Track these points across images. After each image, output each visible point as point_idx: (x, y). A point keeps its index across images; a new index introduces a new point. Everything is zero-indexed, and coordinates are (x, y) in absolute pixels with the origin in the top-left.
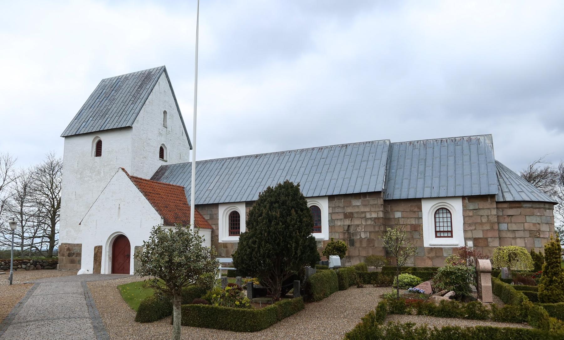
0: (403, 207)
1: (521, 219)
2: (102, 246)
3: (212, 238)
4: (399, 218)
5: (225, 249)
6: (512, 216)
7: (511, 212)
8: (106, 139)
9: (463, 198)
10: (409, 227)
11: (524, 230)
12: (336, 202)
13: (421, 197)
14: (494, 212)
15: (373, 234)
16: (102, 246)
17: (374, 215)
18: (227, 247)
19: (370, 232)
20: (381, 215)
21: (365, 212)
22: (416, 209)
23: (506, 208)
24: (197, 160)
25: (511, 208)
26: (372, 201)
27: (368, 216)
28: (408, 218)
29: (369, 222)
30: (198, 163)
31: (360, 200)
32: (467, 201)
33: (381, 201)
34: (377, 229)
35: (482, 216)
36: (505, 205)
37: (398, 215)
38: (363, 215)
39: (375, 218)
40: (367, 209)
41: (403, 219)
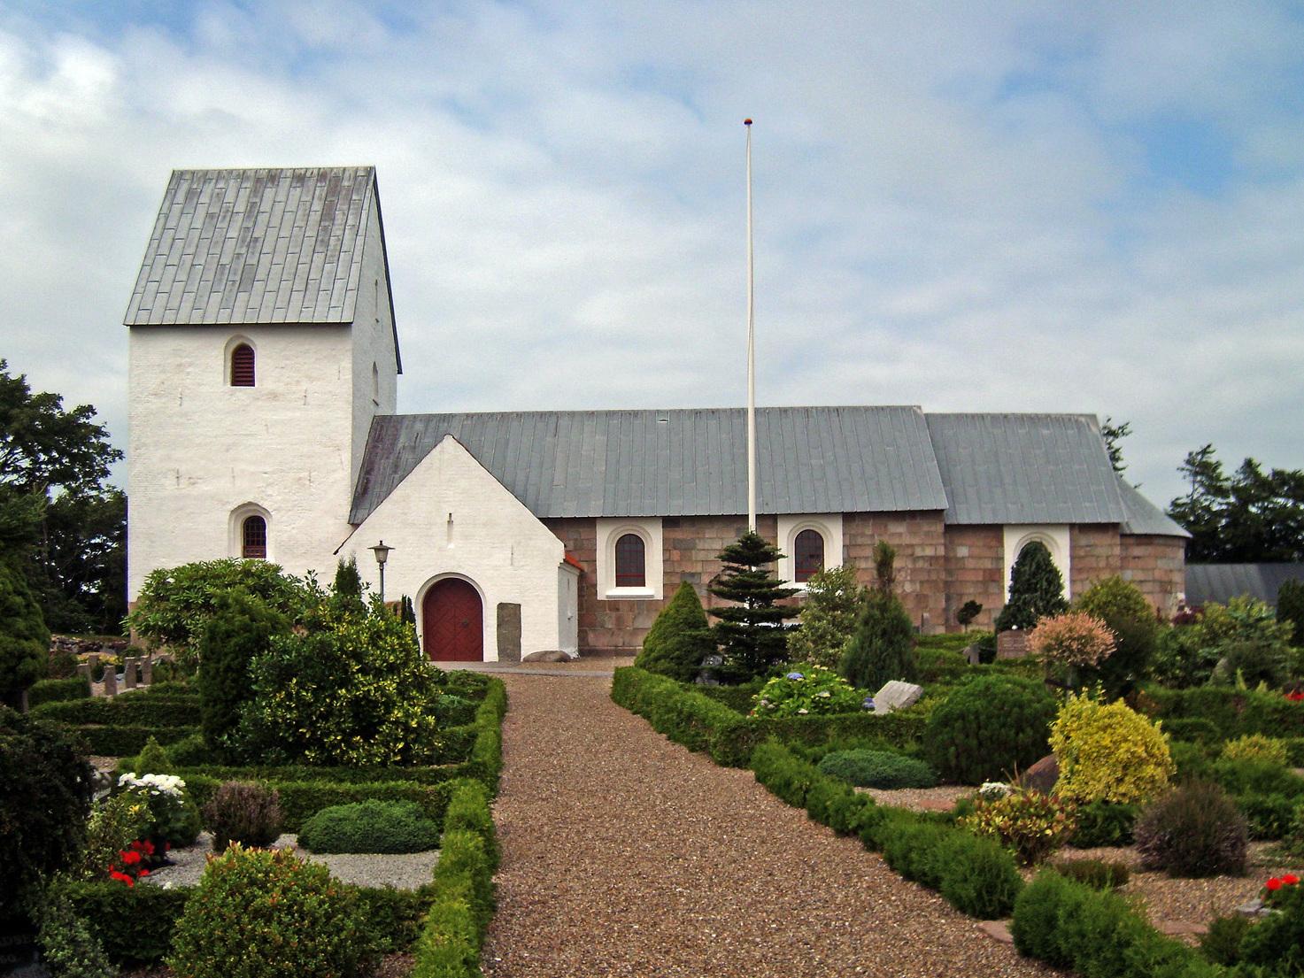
0: (970, 539)
1: (1151, 563)
2: (643, 584)
3: (580, 589)
4: (963, 558)
5: (614, 614)
6: (1138, 557)
7: (1137, 551)
8: (267, 356)
9: (1072, 526)
10: (981, 573)
11: (1154, 581)
12: (856, 527)
13: (1005, 522)
14: (1117, 551)
15: (925, 585)
16: (643, 584)
17: (929, 552)
18: (618, 610)
19: (922, 582)
20: (941, 551)
21: (912, 546)
22: (993, 543)
23: (1133, 545)
24: (762, 404)
25: (1138, 545)
26: (925, 526)
27: (919, 552)
28: (980, 558)
29: (920, 564)
30: (757, 411)
31: (905, 524)
32: (1076, 532)
33: (940, 528)
34: (934, 577)
35: (1098, 557)
36: (1131, 541)
37: (963, 551)
38: (909, 551)
39: (931, 558)
40: (916, 541)
41: (970, 560)
